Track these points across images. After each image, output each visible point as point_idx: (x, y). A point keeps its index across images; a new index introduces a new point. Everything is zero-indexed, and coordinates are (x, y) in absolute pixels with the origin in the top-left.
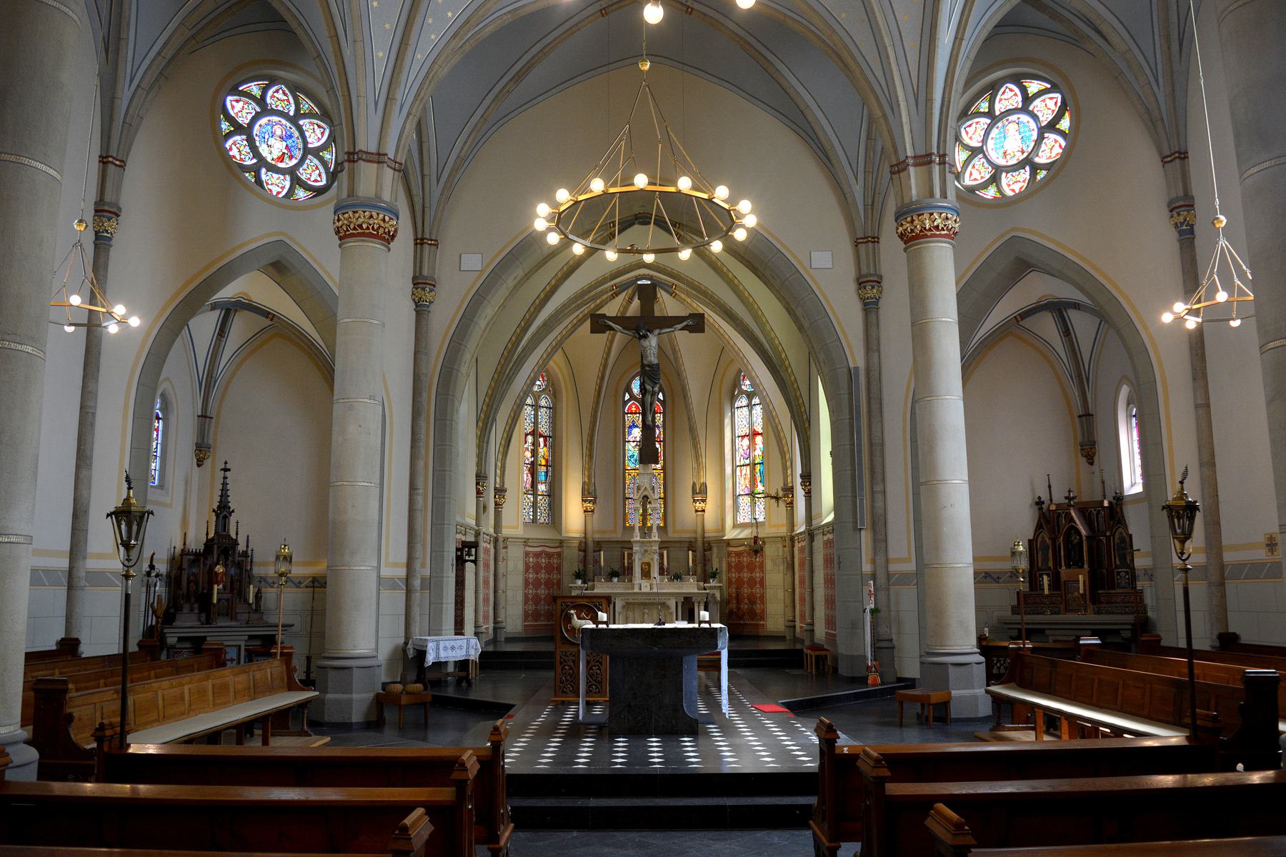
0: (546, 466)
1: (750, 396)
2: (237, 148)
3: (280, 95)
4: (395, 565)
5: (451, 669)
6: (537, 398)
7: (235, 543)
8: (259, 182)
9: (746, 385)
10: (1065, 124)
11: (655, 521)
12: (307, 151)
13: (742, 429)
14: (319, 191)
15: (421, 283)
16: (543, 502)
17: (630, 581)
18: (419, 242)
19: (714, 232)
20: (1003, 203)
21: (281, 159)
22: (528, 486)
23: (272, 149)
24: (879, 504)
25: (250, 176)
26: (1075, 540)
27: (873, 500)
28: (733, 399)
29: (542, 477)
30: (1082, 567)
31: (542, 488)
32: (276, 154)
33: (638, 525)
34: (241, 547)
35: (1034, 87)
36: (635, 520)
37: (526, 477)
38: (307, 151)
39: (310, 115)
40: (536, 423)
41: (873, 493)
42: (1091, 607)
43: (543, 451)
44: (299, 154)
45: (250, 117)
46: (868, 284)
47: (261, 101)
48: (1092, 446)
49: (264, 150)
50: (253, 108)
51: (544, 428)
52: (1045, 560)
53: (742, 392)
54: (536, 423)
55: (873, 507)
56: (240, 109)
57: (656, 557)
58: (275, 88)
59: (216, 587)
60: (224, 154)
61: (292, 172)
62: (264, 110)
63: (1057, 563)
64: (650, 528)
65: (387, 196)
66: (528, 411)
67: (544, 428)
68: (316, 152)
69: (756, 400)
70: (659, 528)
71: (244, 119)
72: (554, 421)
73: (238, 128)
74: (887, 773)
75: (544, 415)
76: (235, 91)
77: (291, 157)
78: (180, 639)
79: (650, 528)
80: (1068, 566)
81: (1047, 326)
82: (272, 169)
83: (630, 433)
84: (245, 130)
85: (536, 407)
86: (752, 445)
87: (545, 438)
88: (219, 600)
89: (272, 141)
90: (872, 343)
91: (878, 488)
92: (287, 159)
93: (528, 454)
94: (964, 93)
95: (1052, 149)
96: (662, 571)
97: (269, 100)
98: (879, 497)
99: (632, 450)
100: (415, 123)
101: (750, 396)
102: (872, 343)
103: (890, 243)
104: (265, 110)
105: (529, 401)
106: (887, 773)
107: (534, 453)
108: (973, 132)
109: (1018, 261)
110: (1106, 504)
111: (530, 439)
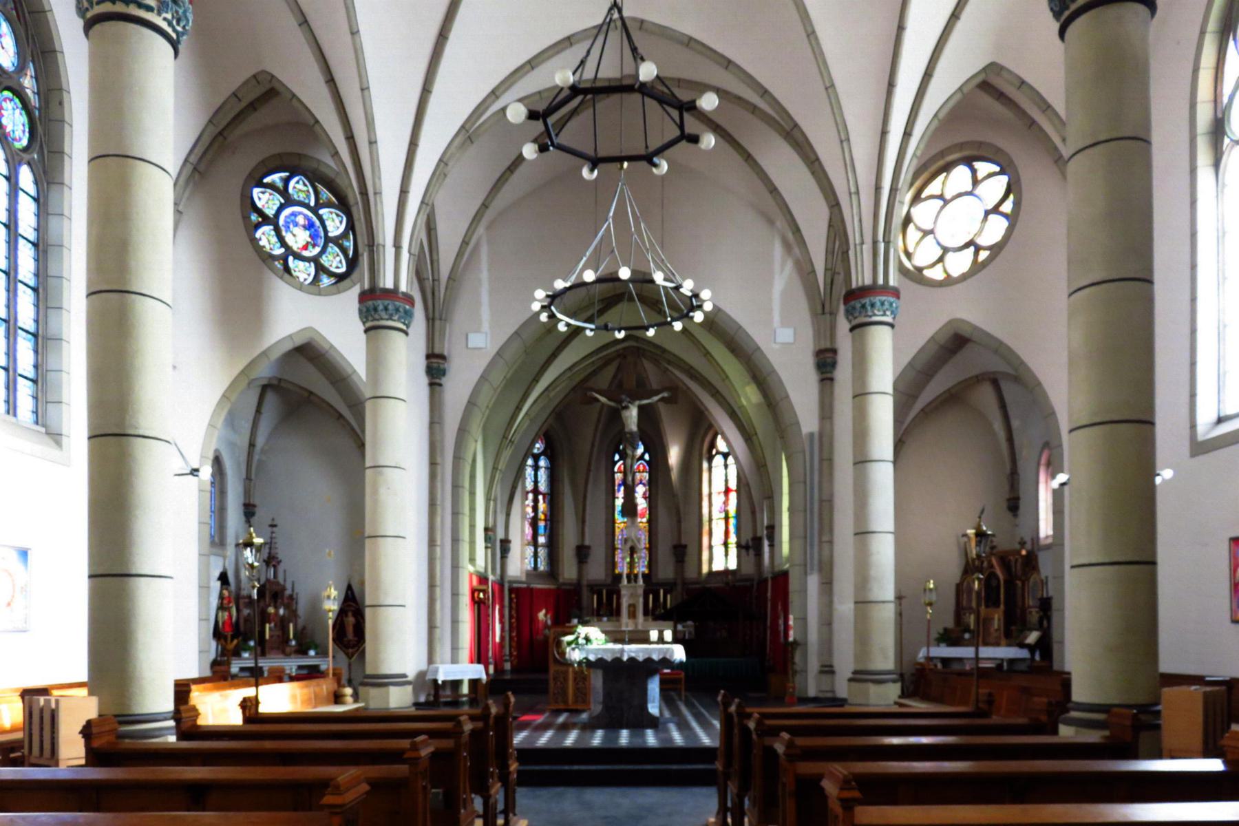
1: (725, 456)
2: (265, 236)
3: (300, 186)
4: (446, 673)
5: (465, 689)
6: (536, 458)
7: (284, 589)
8: (287, 269)
9: (721, 445)
10: (1007, 207)
11: (642, 568)
12: (328, 240)
13: (718, 486)
14: (340, 278)
15: (436, 367)
16: (542, 552)
17: (618, 621)
18: (431, 320)
19: (693, 308)
20: (949, 281)
21: (305, 248)
22: (529, 538)
23: (298, 238)
24: (826, 552)
25: (279, 265)
26: (994, 583)
27: (820, 549)
28: (710, 459)
29: (541, 531)
30: (998, 606)
31: (542, 540)
32: (301, 244)
33: (626, 571)
34: (288, 592)
35: (983, 168)
36: (623, 568)
37: (528, 530)
38: (328, 240)
39: (328, 205)
40: (536, 482)
41: (821, 542)
42: (1003, 641)
43: (542, 506)
44: (321, 242)
45: (275, 208)
46: (825, 362)
47: (284, 192)
48: (1016, 502)
49: (289, 239)
50: (278, 200)
52: (970, 600)
53: (718, 453)
54: (536, 482)
55: (820, 555)
56: (266, 201)
57: (641, 600)
58: (296, 179)
59: (267, 626)
60: (254, 242)
61: (315, 260)
62: (289, 201)
63: (979, 605)
64: (636, 576)
65: (403, 288)
66: (529, 471)
67: (543, 487)
68: (337, 241)
69: (731, 460)
70: (644, 575)
71: (270, 212)
73: (266, 220)
74: (856, 794)
75: (543, 475)
76: (260, 184)
77: (314, 246)
78: (242, 669)
79: (636, 576)
80: (987, 606)
81: (985, 396)
82: (298, 257)
84: (273, 221)
85: (536, 468)
86: (726, 503)
87: (544, 495)
88: (271, 636)
89: (296, 230)
90: (826, 411)
91: (825, 538)
92: (310, 247)
93: (529, 510)
94: (911, 185)
95: (996, 229)
96: (646, 613)
97: (291, 190)
98: (826, 547)
99: (619, 502)
100: (425, 217)
101: (725, 456)
102: (826, 411)
103: (843, 325)
104: (289, 201)
105: (530, 462)
106: (856, 794)
107: (535, 508)
108: (923, 214)
109: (956, 342)
110: (1024, 552)
111: (531, 496)
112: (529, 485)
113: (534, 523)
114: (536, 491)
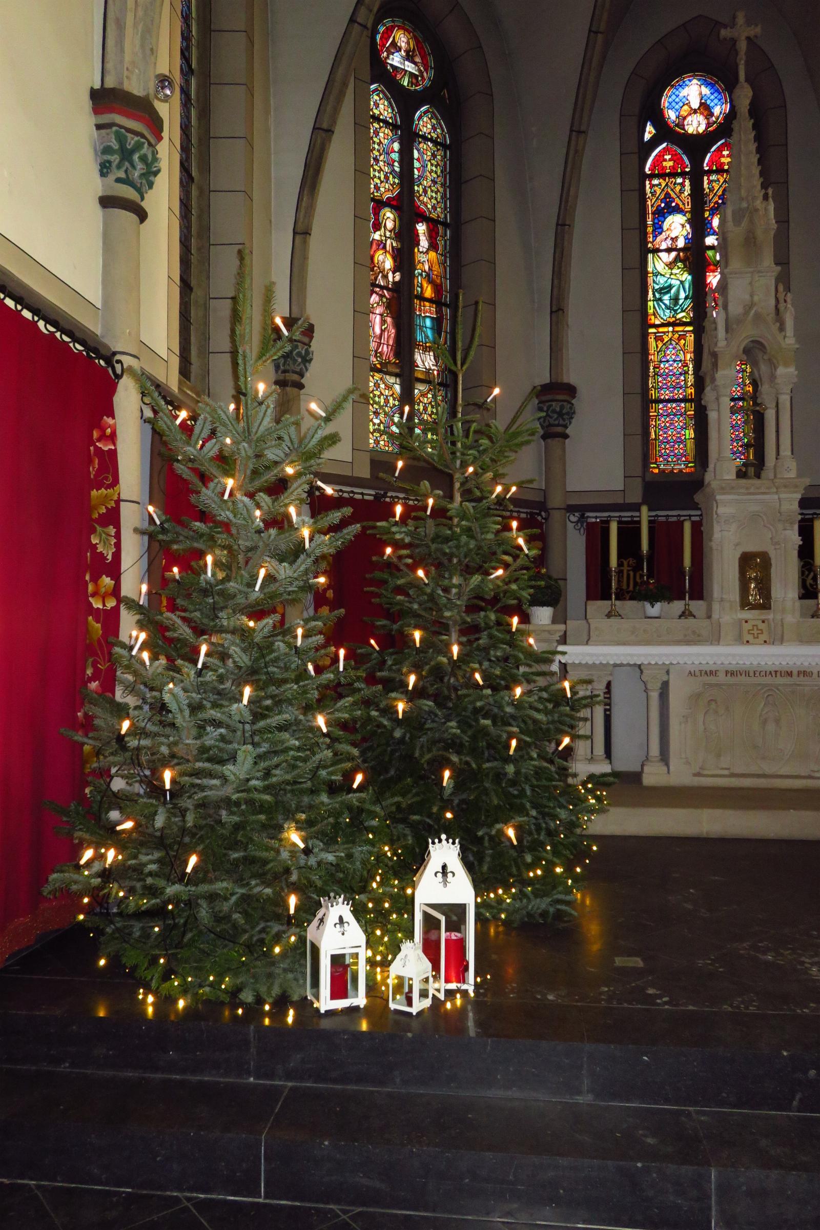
0: (437, 301)
40: (406, 177)
43: (426, 258)
51: (430, 196)
54: (406, 177)
67: (430, 196)
72: (456, 180)
75: (427, 163)
83: (658, 229)
85: (408, 137)
87: (433, 224)
107: (404, 259)
112: (383, 183)
113: (401, 302)
114: (406, 205)
